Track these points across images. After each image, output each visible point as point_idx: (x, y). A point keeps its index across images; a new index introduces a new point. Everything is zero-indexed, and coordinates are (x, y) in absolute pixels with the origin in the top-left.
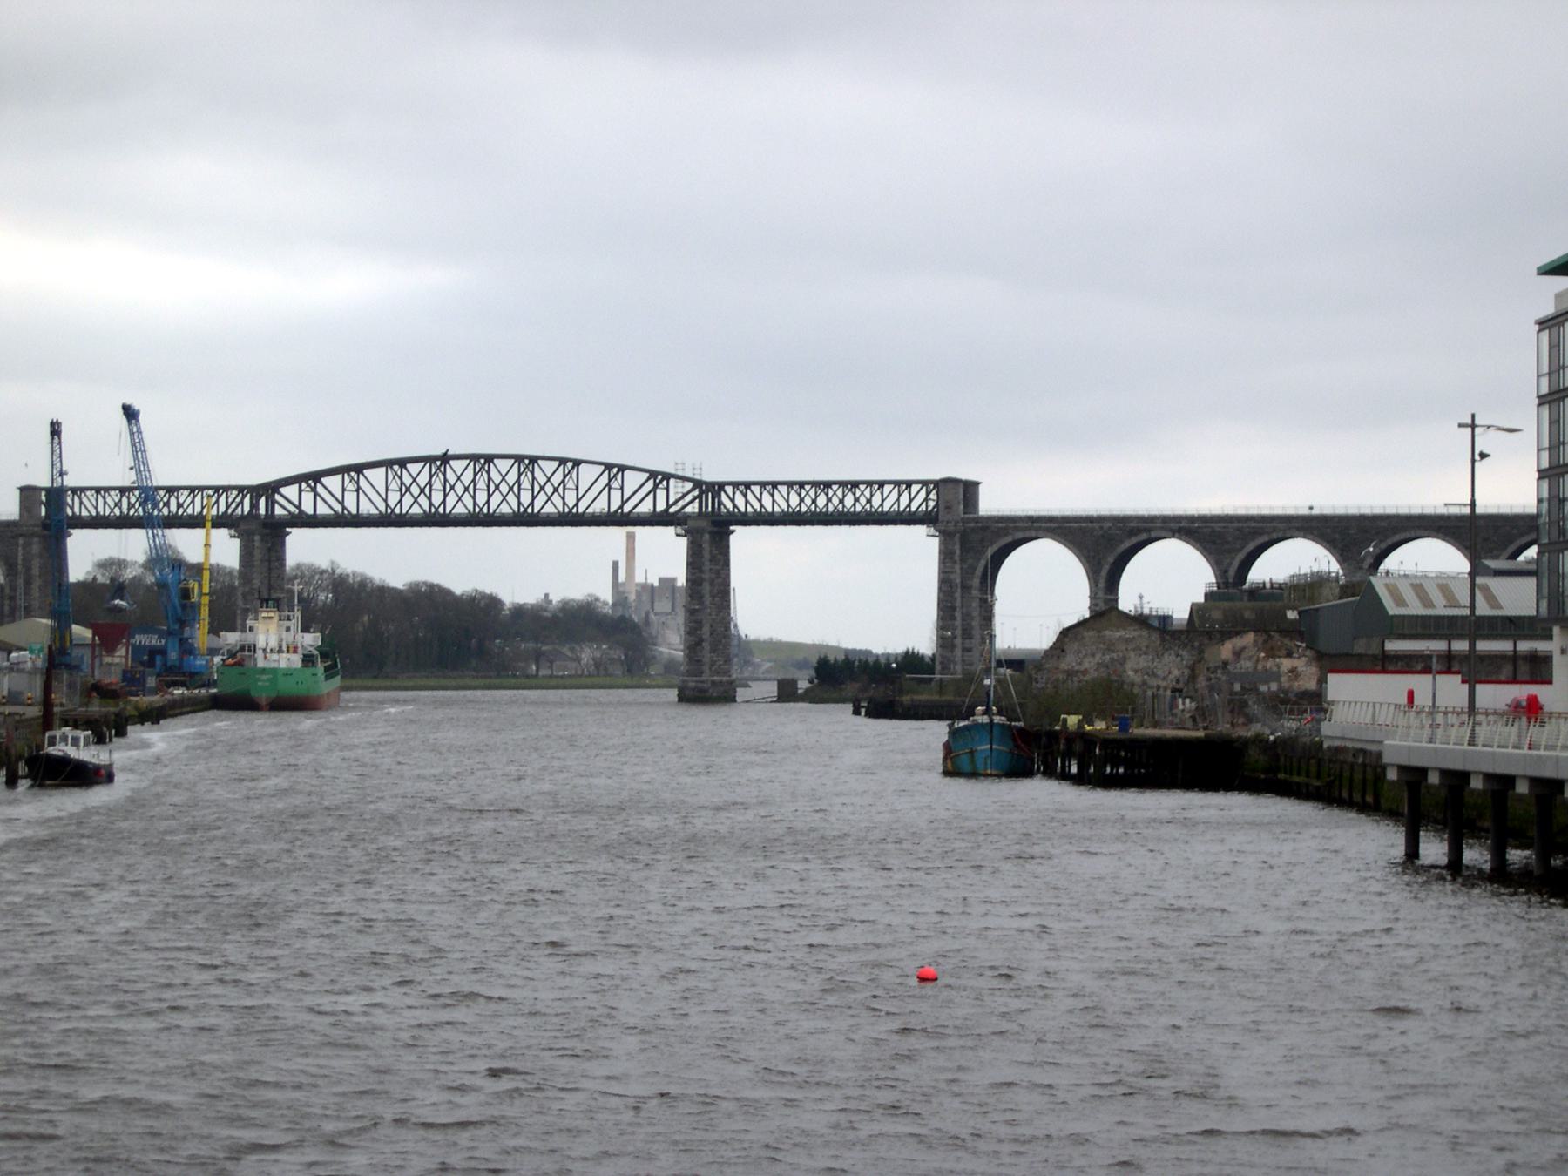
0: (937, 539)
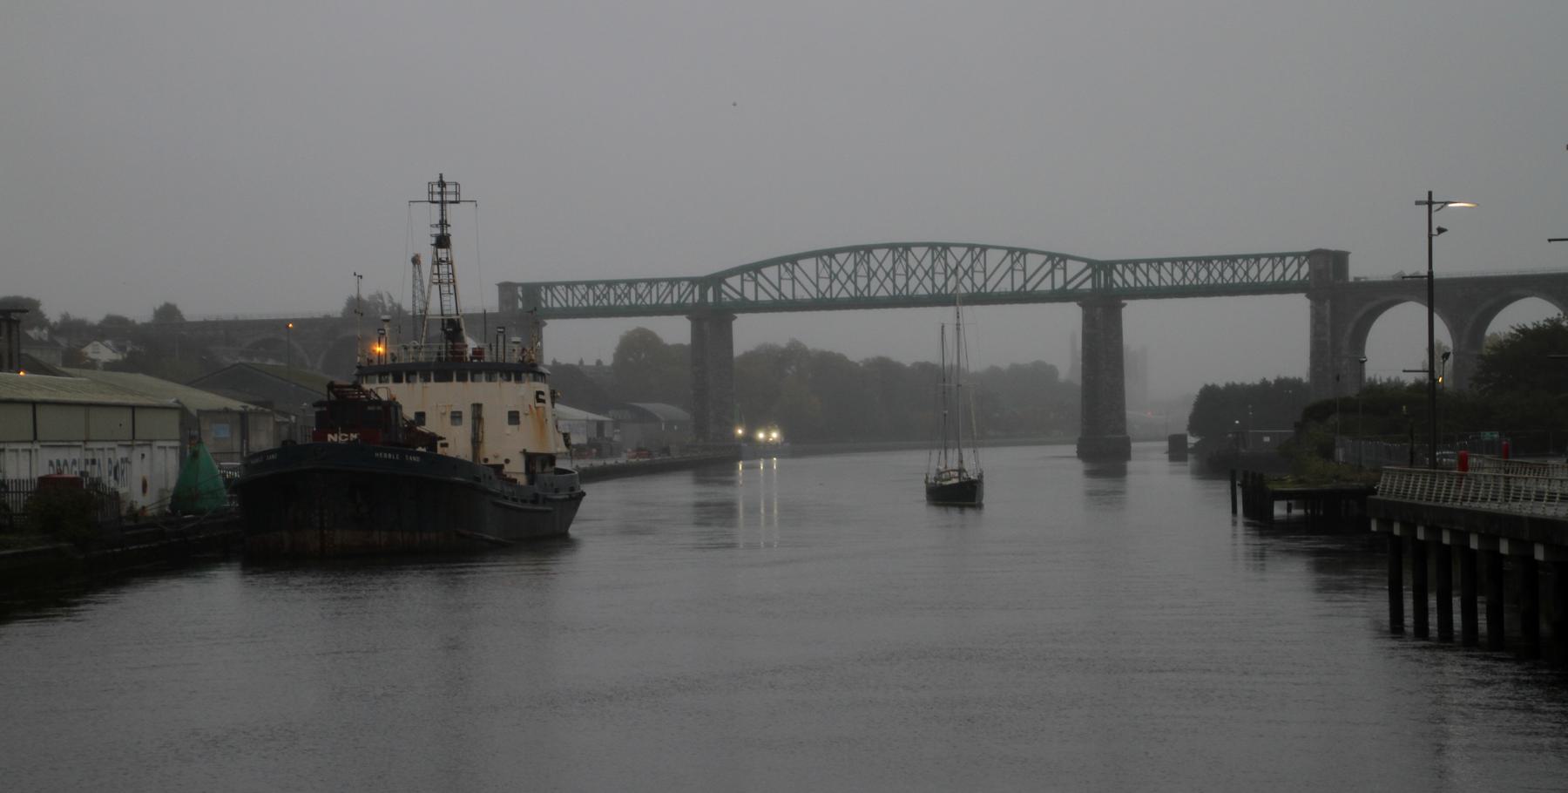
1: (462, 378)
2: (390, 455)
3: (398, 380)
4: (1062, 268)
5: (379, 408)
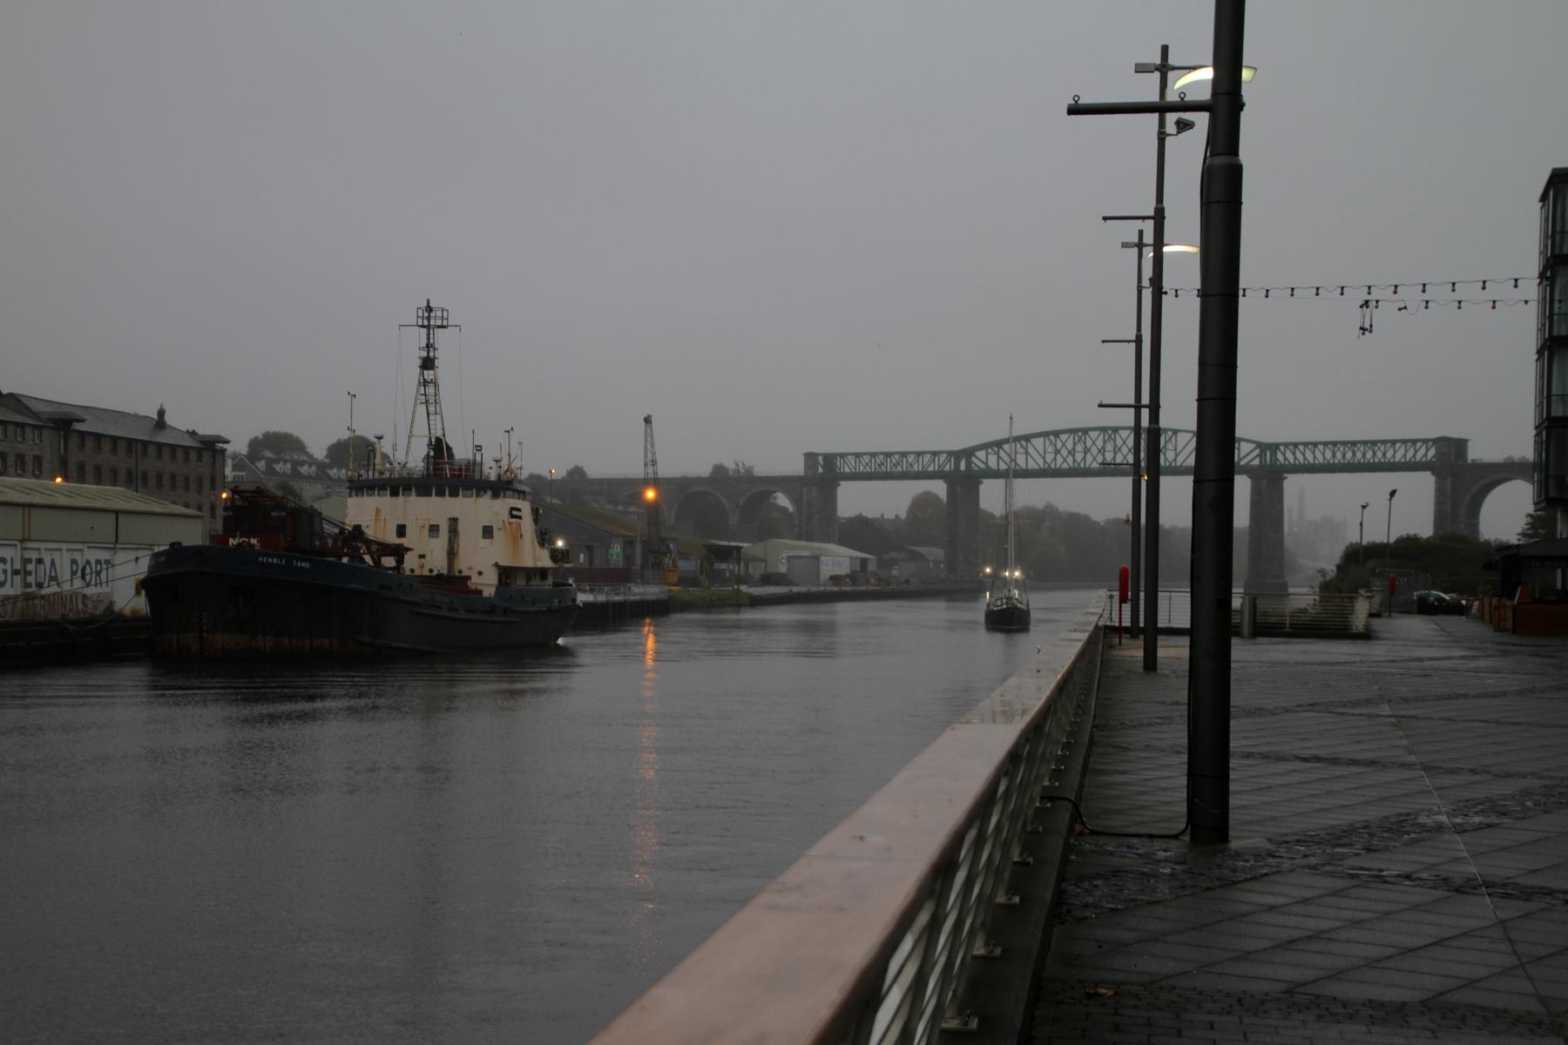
1: (440, 493)
2: (275, 560)
3: (395, 493)
5: (283, 514)
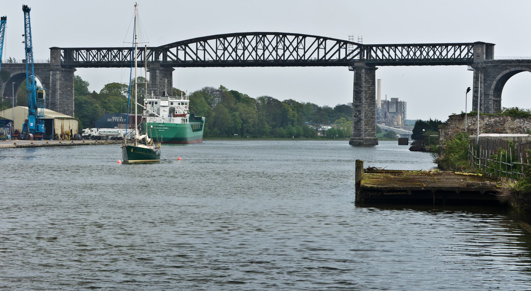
0: (472, 72)
4: (345, 48)
